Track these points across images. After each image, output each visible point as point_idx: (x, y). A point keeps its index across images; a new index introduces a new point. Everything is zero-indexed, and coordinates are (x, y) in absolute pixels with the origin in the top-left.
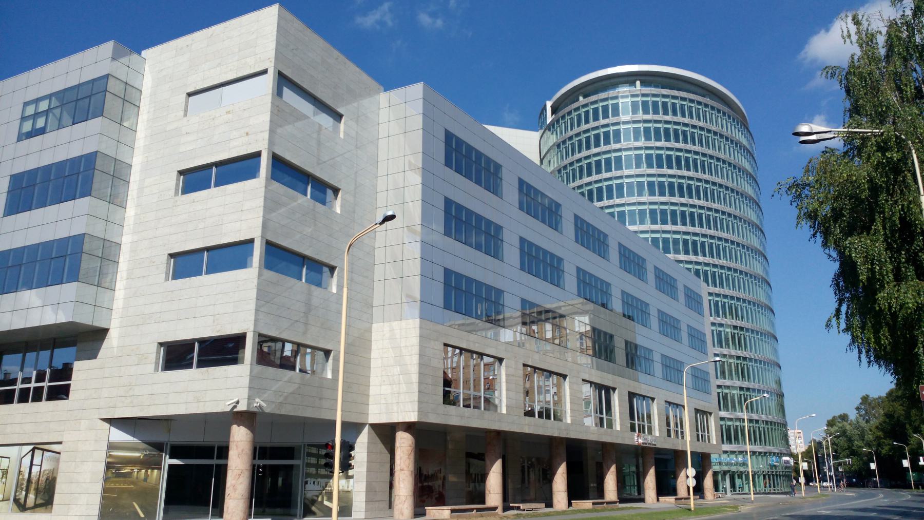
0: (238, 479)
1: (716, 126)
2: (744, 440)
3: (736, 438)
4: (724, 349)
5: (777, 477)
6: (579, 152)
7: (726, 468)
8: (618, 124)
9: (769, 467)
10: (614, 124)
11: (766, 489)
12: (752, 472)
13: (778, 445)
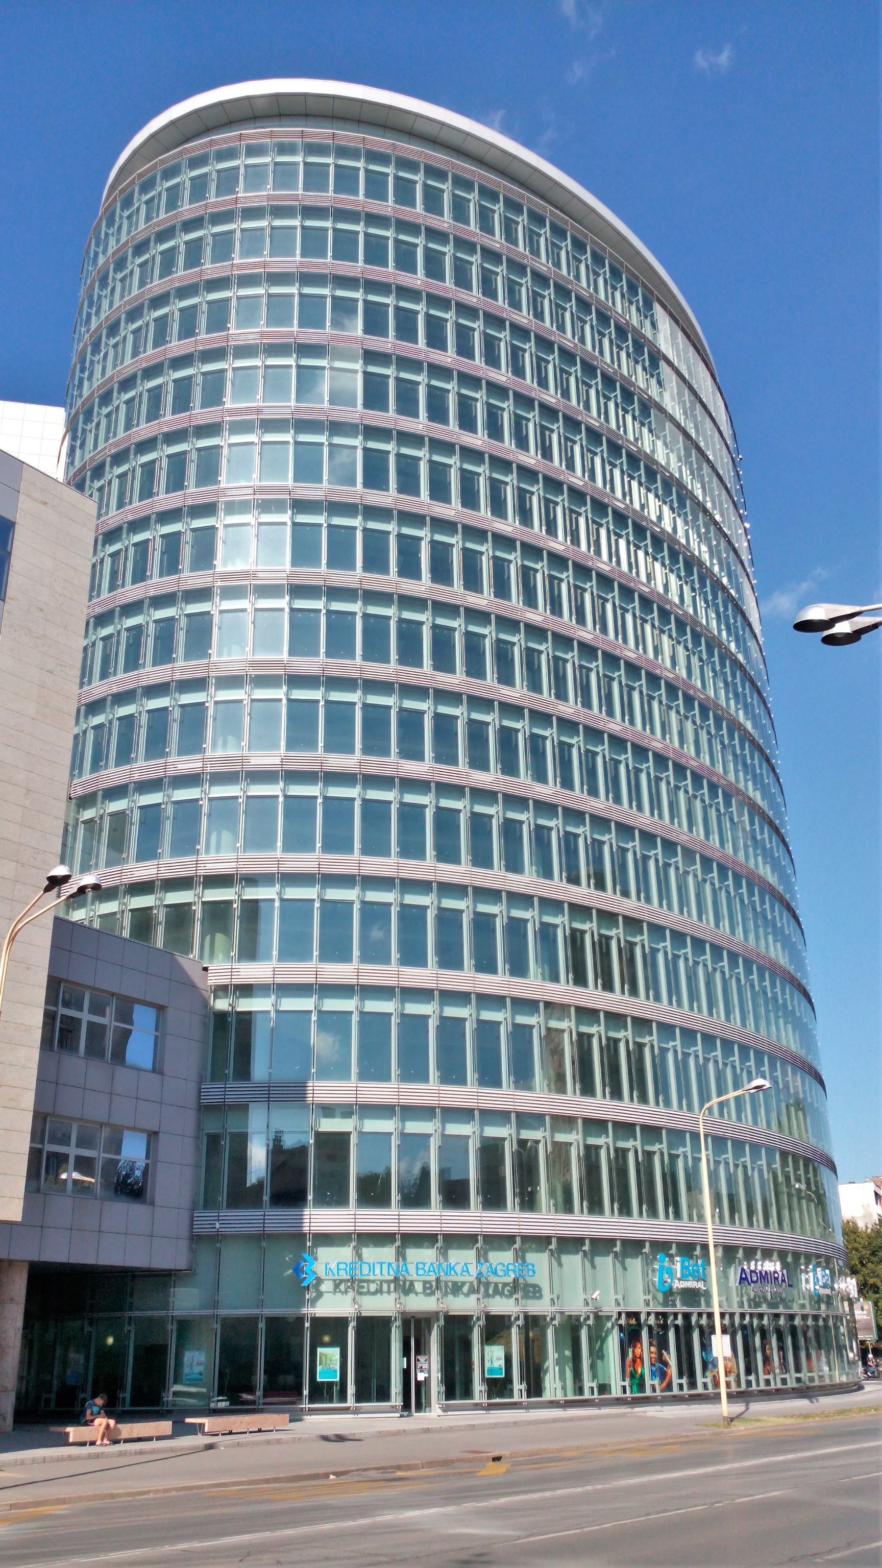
0: (687, 1368)
1: (664, 737)
2: (695, 1204)
3: (672, 1200)
4: (617, 995)
5: (780, 1338)
6: (104, 675)
7: (420, 1303)
8: (199, 684)
9: (807, 1302)
10: (187, 685)
11: (770, 1377)
12: (722, 1315)
13: (808, 1229)
